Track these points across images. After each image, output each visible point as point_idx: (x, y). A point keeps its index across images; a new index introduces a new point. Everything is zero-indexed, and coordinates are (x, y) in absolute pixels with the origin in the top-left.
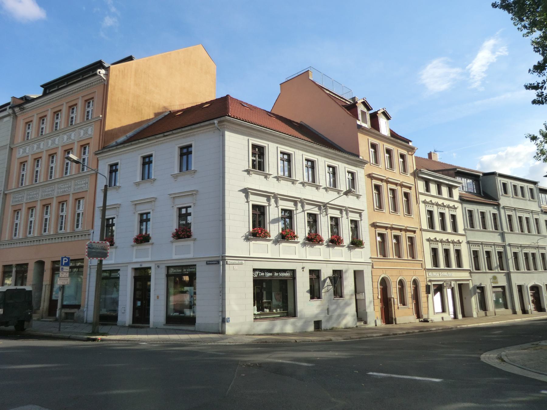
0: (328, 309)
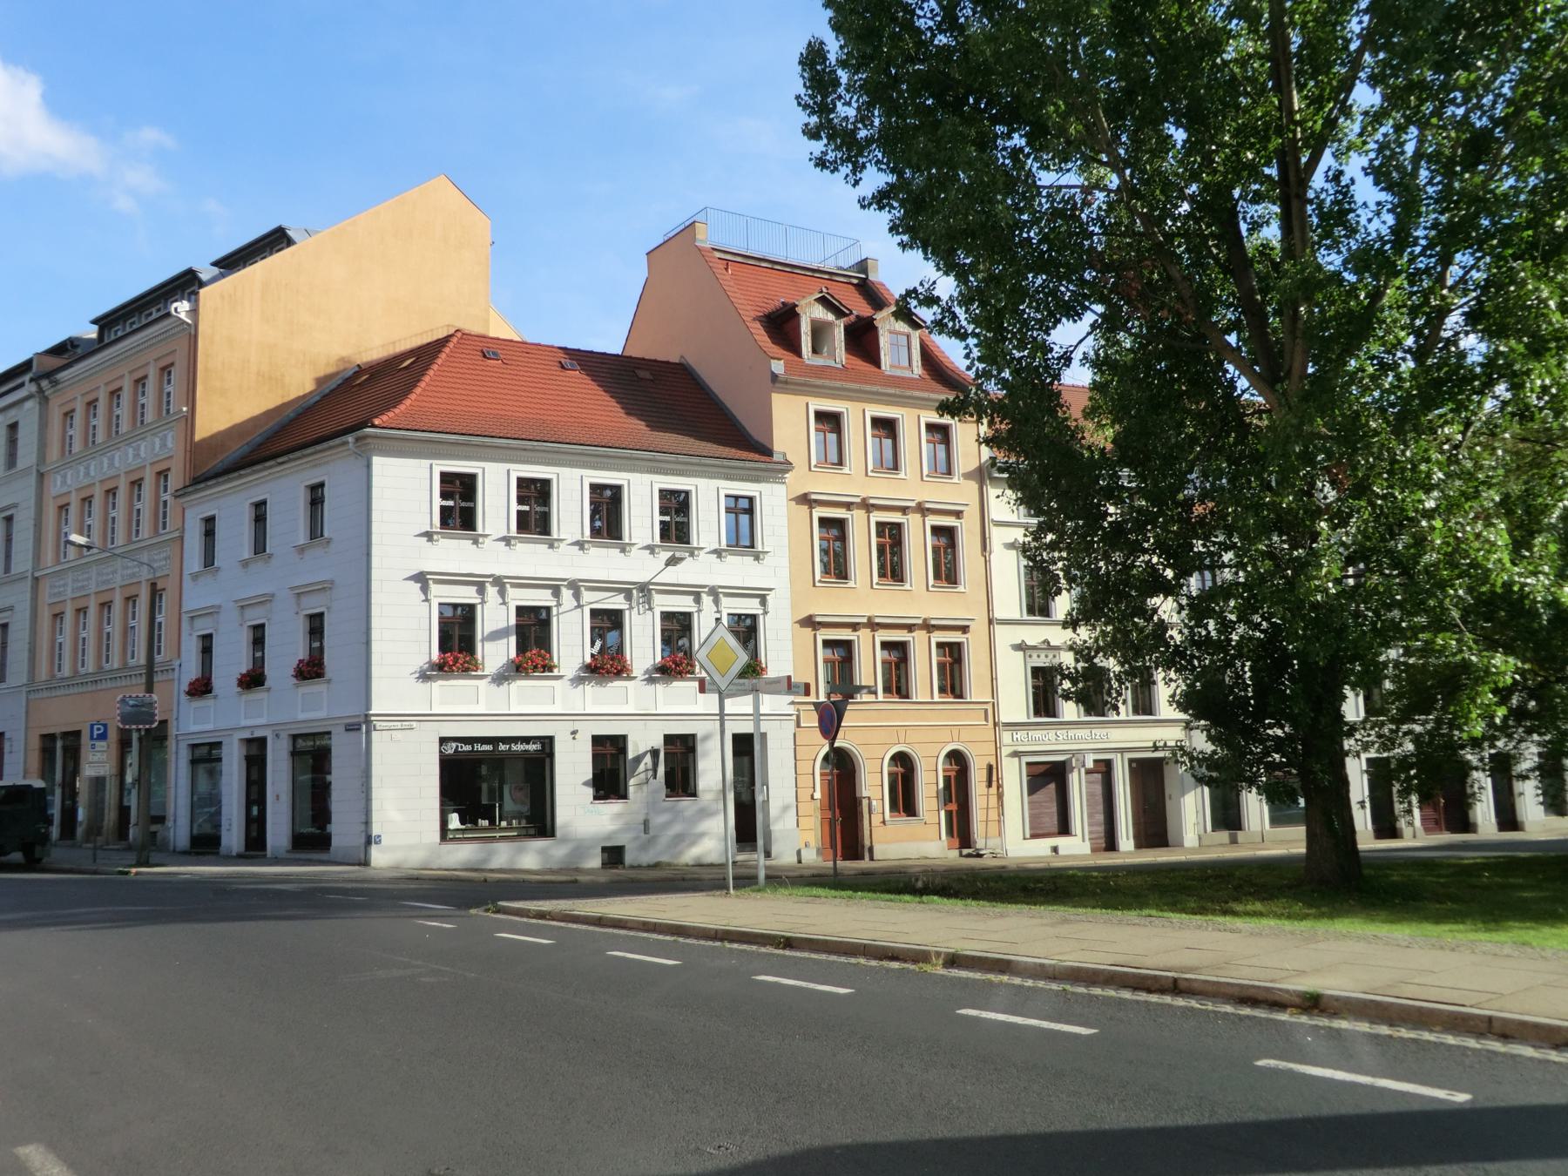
0: (646, 823)
